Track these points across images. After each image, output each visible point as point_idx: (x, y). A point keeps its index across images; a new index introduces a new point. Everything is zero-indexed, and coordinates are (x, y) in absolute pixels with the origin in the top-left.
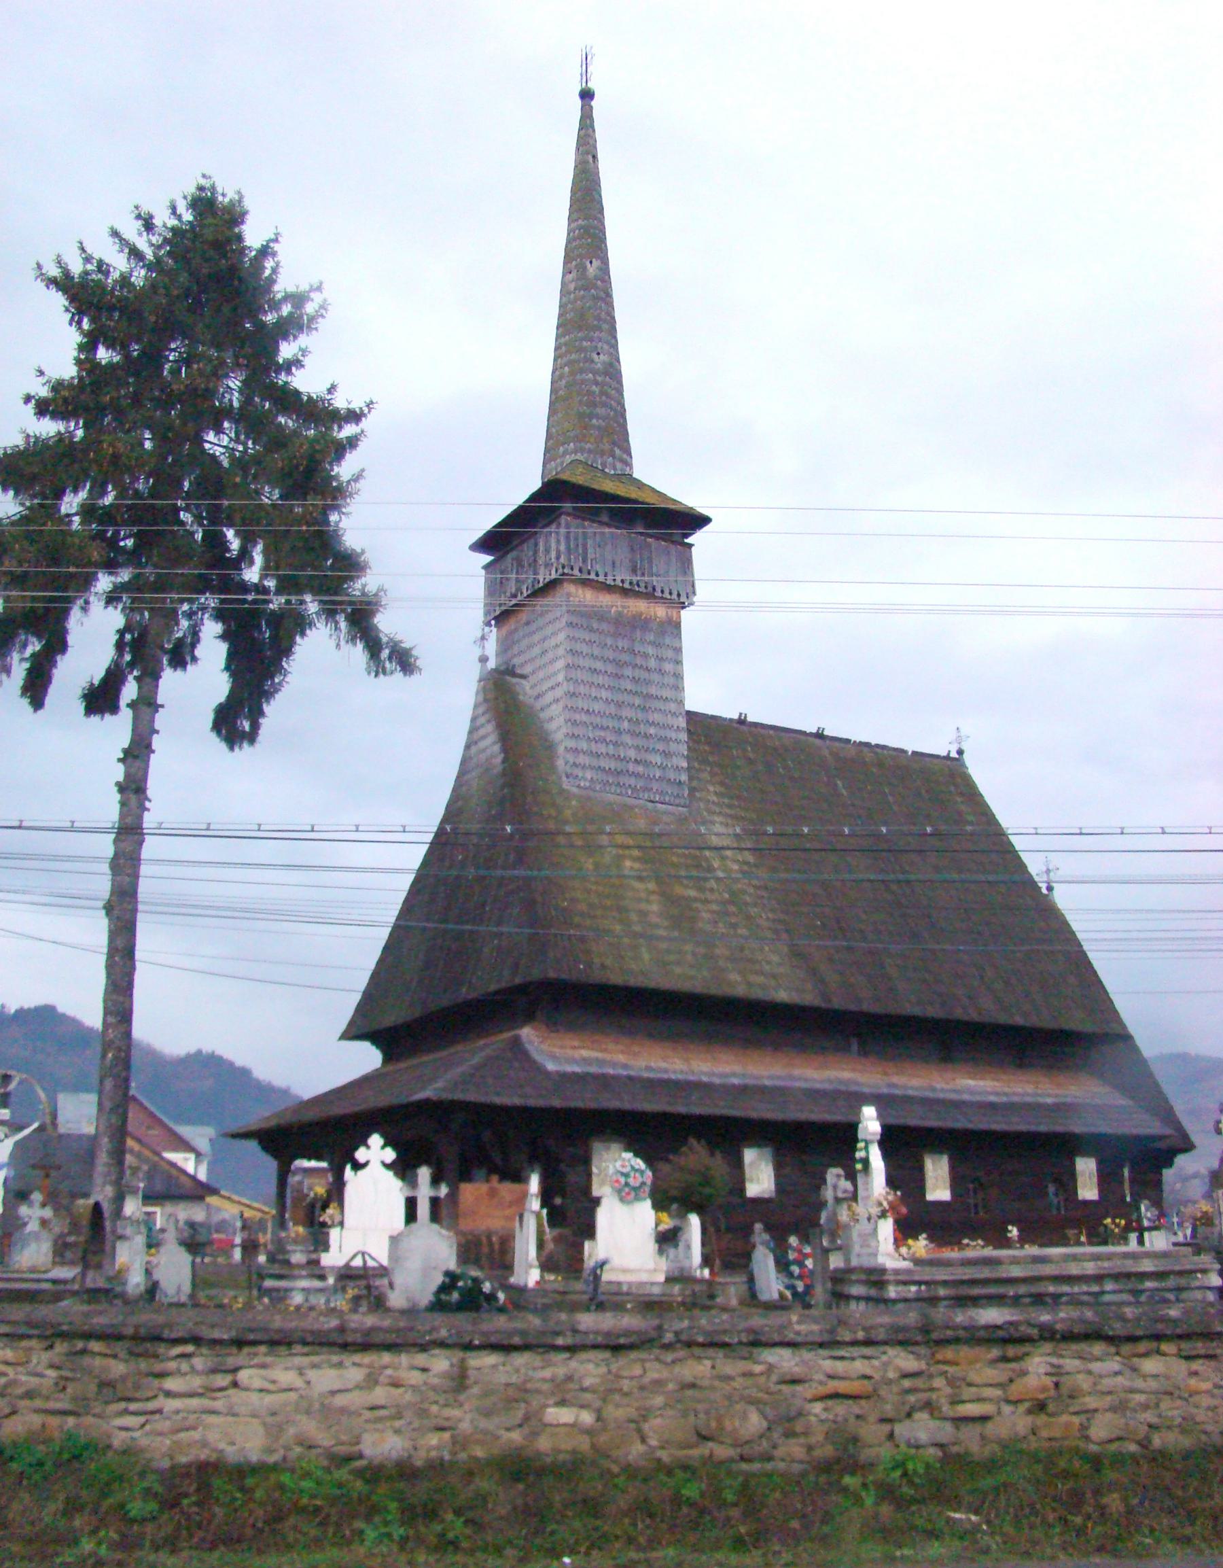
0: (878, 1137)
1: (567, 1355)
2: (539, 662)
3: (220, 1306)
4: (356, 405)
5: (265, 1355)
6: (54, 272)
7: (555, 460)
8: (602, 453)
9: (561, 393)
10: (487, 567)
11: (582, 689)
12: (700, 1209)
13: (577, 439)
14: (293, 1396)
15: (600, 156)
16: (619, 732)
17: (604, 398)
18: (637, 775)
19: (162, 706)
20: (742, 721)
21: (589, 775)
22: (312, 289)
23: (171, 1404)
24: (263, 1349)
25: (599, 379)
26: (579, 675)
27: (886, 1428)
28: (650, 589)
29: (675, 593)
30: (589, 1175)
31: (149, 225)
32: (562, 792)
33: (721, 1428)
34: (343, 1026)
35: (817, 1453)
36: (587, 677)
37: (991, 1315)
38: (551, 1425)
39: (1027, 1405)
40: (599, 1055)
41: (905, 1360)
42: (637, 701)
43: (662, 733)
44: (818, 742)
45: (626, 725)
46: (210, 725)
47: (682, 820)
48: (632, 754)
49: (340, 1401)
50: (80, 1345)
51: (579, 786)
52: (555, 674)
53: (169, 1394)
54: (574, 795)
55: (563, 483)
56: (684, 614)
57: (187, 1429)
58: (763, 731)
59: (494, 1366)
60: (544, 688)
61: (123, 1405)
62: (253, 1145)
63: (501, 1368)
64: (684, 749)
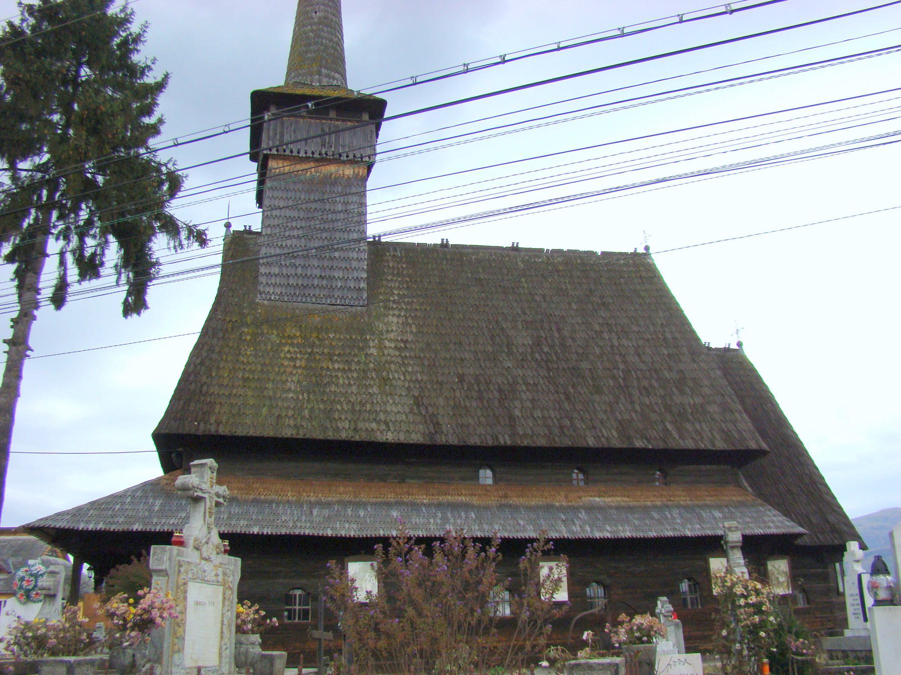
3: (432, 586)
18: (322, 287)
21: (278, 290)
25: (314, 28)
43: (345, 255)
44: (512, 253)
46: (752, 355)
48: (318, 272)
51: (270, 300)
58: (463, 250)
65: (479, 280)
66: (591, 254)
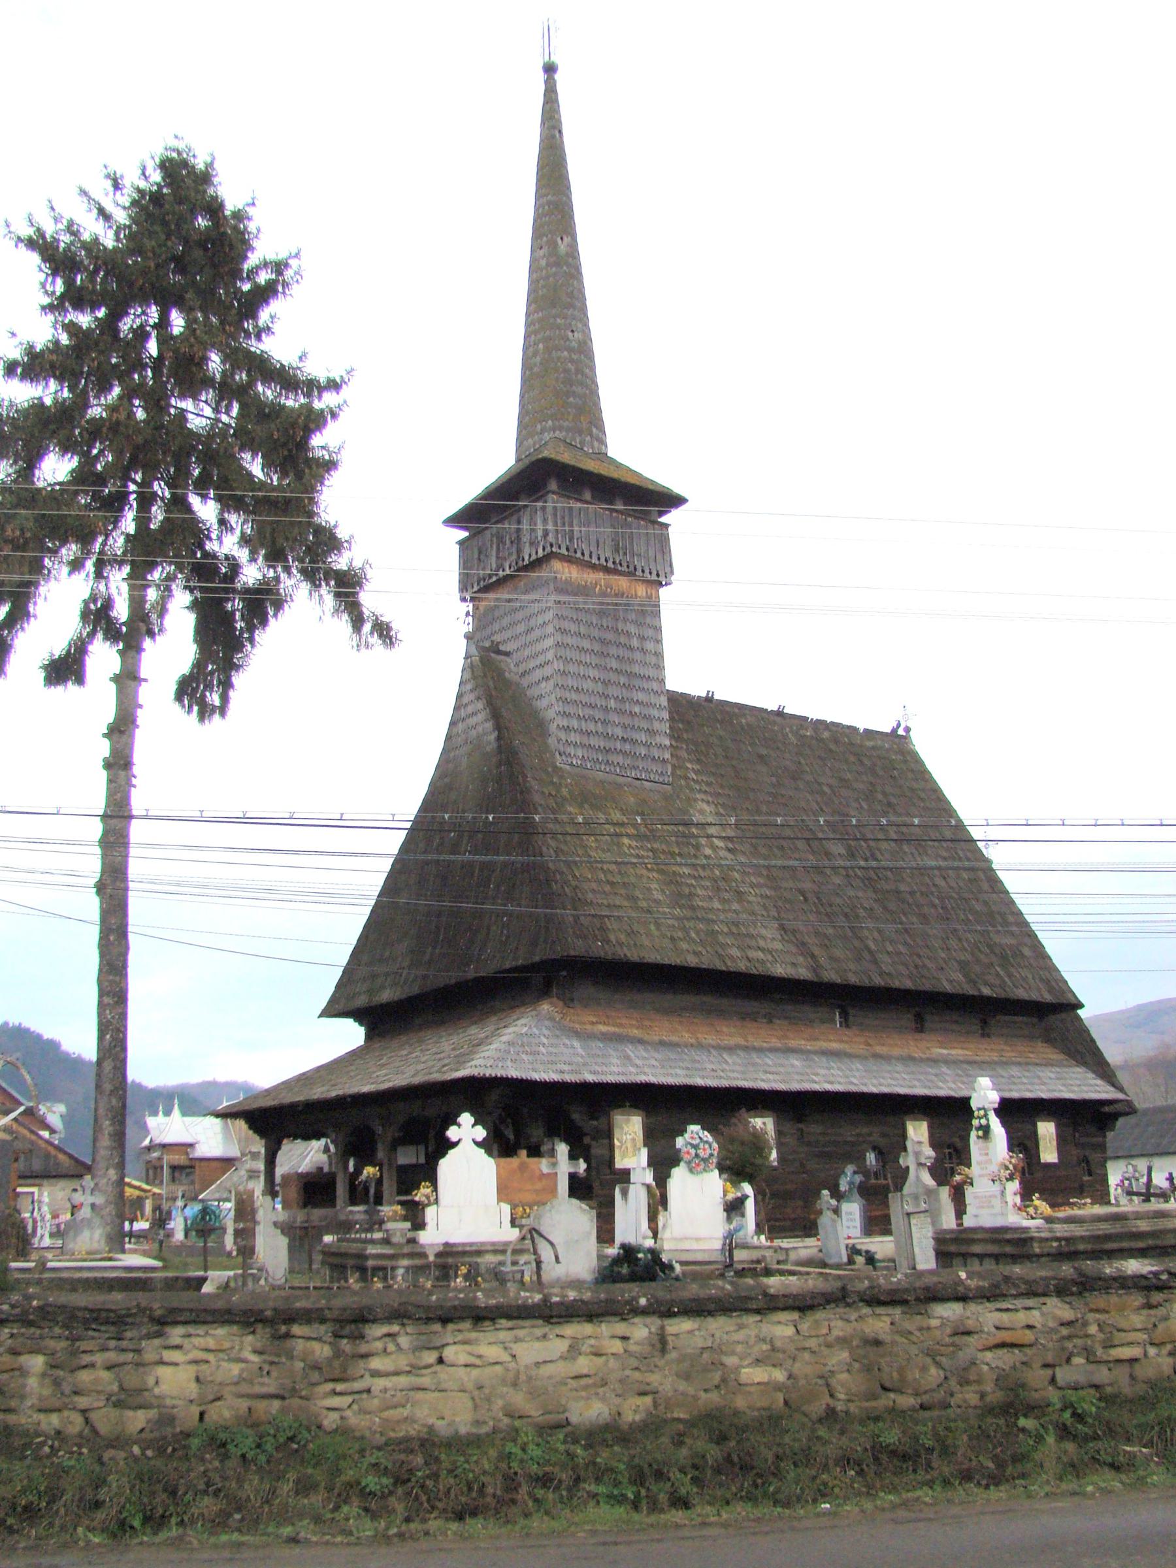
0: (996, 1106)
1: (758, 1318)
2: (523, 640)
4: (336, 375)
5: (469, 1330)
6: (28, 232)
7: (532, 437)
8: (580, 432)
9: (536, 370)
10: (461, 543)
11: (572, 668)
12: (751, 1179)
13: (553, 417)
14: (498, 1368)
15: (564, 131)
16: (606, 709)
17: (580, 376)
19: (145, 680)
20: (709, 699)
22: (290, 257)
23: (379, 1383)
24: (467, 1325)
25: (575, 357)
26: (569, 654)
27: (1049, 1372)
28: (632, 568)
29: (654, 573)
30: (611, 1148)
31: (117, 186)
32: (556, 769)
33: (903, 1379)
34: (323, 1004)
35: (988, 1399)
36: (575, 655)
37: (1133, 1266)
38: (746, 1385)
39: (1169, 1347)
40: (612, 1029)
41: (1058, 1309)
42: (622, 680)
43: (646, 711)
44: (778, 719)
45: (612, 704)
47: (666, 798)
48: (619, 732)
49: (546, 1370)
50: (283, 1329)
52: (544, 652)
53: (376, 1374)
54: (569, 773)
55: (546, 461)
56: (663, 591)
57: (396, 1407)
59: (691, 1332)
60: (532, 664)
61: (330, 1386)
62: (241, 1124)
63: (697, 1333)
64: (665, 727)
65: (761, 757)
66: (854, 729)
